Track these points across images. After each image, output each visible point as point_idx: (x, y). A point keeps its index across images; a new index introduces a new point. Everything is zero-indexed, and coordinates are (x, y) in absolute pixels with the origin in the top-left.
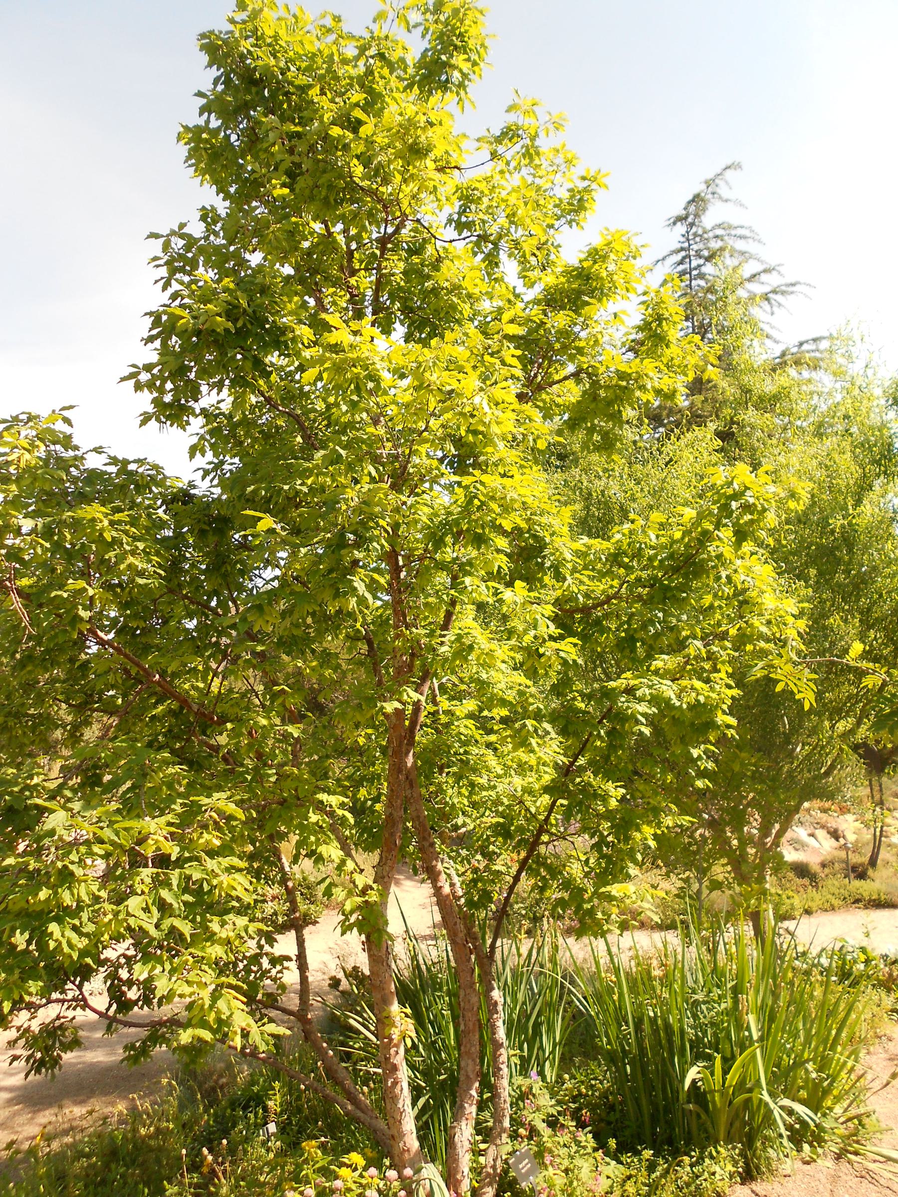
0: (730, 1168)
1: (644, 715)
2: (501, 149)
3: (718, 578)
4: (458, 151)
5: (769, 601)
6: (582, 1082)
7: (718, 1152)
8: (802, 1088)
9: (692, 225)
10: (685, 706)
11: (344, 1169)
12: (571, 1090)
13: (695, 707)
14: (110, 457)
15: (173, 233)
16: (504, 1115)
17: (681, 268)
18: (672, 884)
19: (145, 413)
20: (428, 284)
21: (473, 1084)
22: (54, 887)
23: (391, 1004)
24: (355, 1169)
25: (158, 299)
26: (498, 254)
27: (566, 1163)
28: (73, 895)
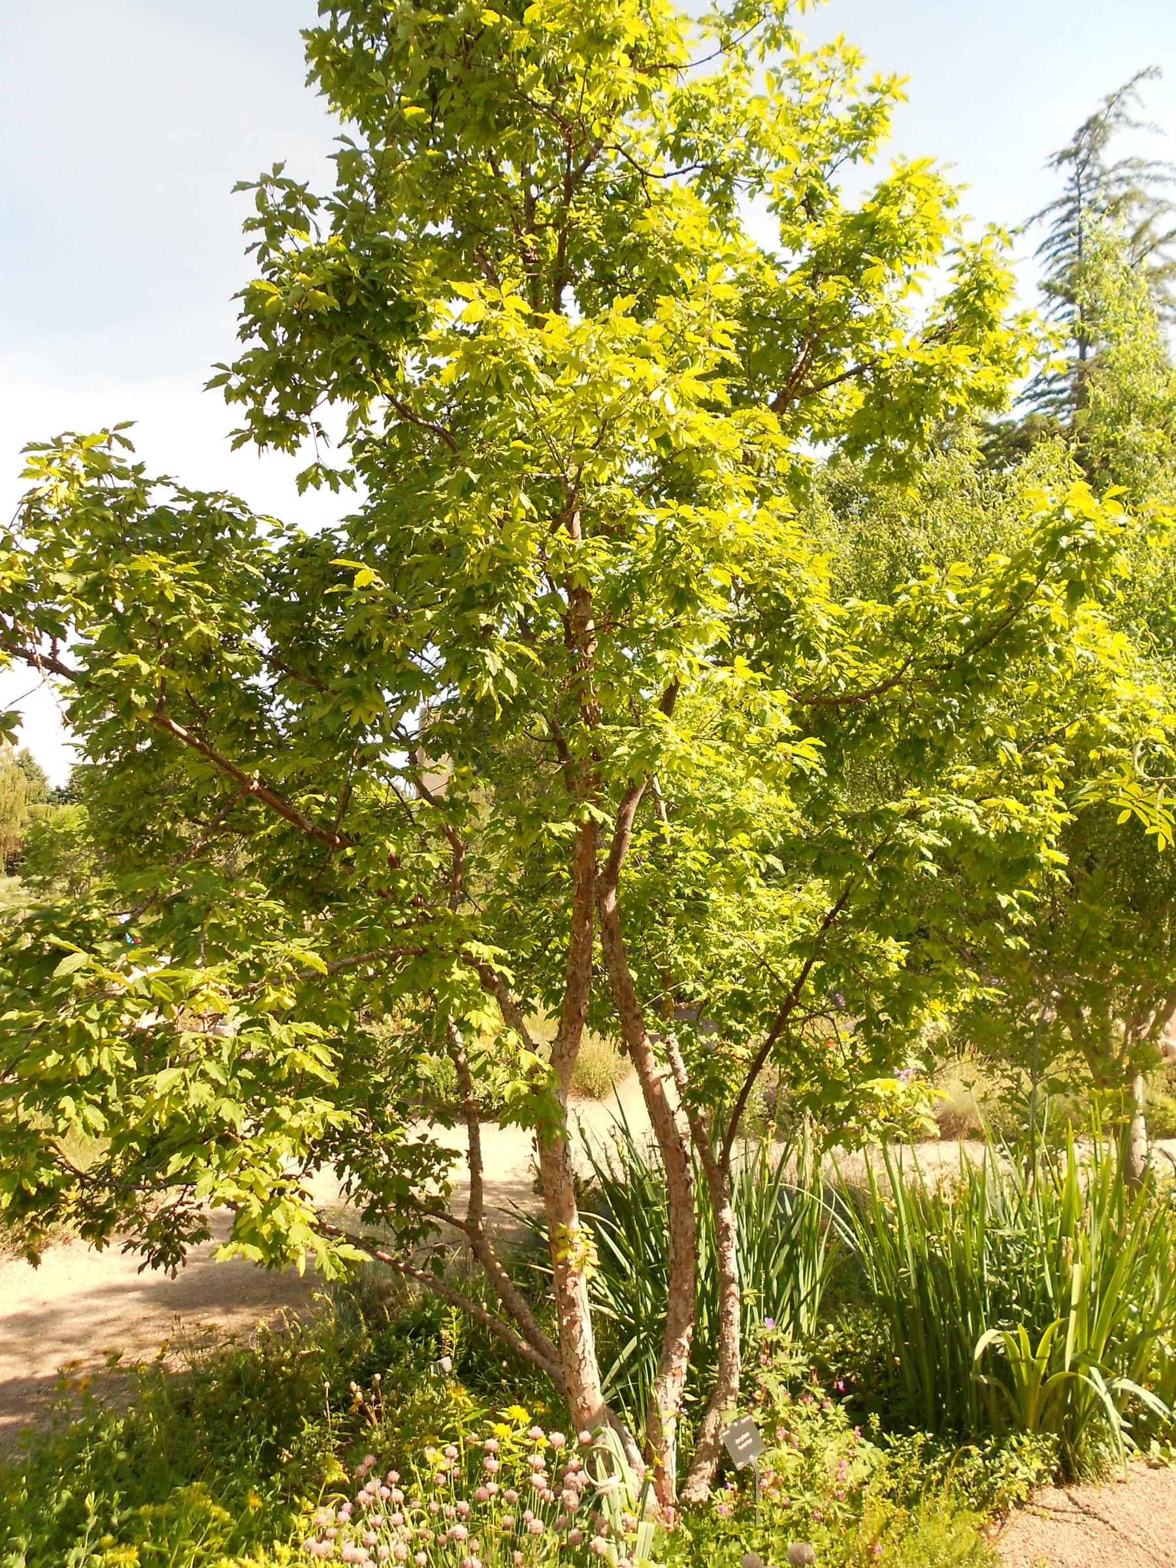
0: (1037, 1464)
1: (931, 847)
2: (735, 34)
3: (1043, 651)
4: (678, 43)
5: (1123, 690)
6: (850, 1336)
7: (1020, 1443)
8: (1155, 1365)
9: (1084, 163)
10: (992, 835)
11: (501, 1425)
12: (833, 1345)
13: (1009, 837)
14: (180, 490)
15: (265, 179)
16: (731, 1373)
17: (1066, 226)
18: (998, 1085)
19: (237, 431)
20: (628, 238)
21: (683, 1329)
22: (64, 1051)
23: (567, 1221)
24: (516, 1428)
25: (251, 273)
26: (732, 193)
27: (807, 1442)
28: (90, 1062)
